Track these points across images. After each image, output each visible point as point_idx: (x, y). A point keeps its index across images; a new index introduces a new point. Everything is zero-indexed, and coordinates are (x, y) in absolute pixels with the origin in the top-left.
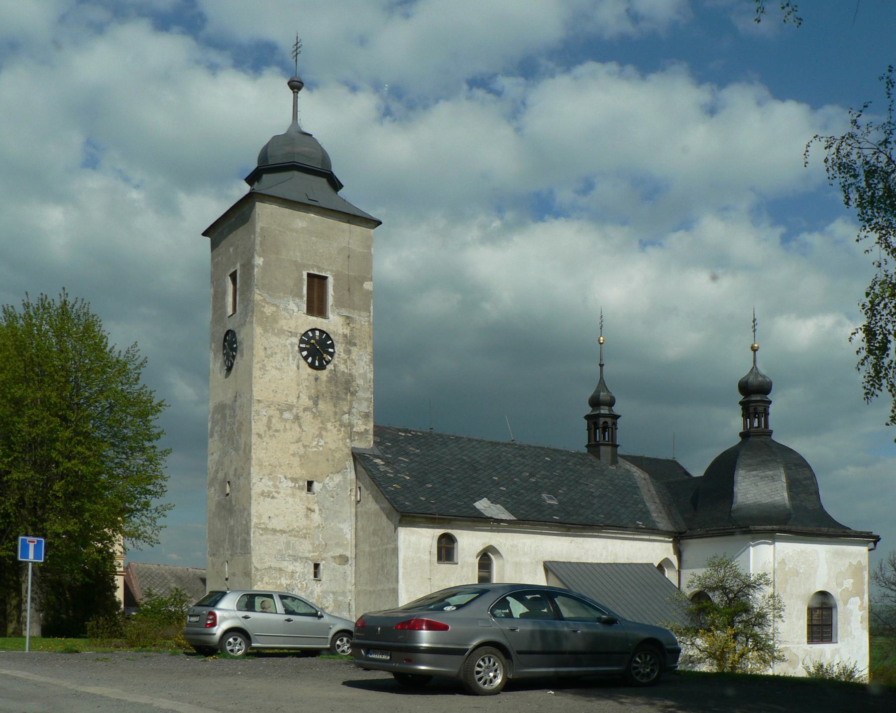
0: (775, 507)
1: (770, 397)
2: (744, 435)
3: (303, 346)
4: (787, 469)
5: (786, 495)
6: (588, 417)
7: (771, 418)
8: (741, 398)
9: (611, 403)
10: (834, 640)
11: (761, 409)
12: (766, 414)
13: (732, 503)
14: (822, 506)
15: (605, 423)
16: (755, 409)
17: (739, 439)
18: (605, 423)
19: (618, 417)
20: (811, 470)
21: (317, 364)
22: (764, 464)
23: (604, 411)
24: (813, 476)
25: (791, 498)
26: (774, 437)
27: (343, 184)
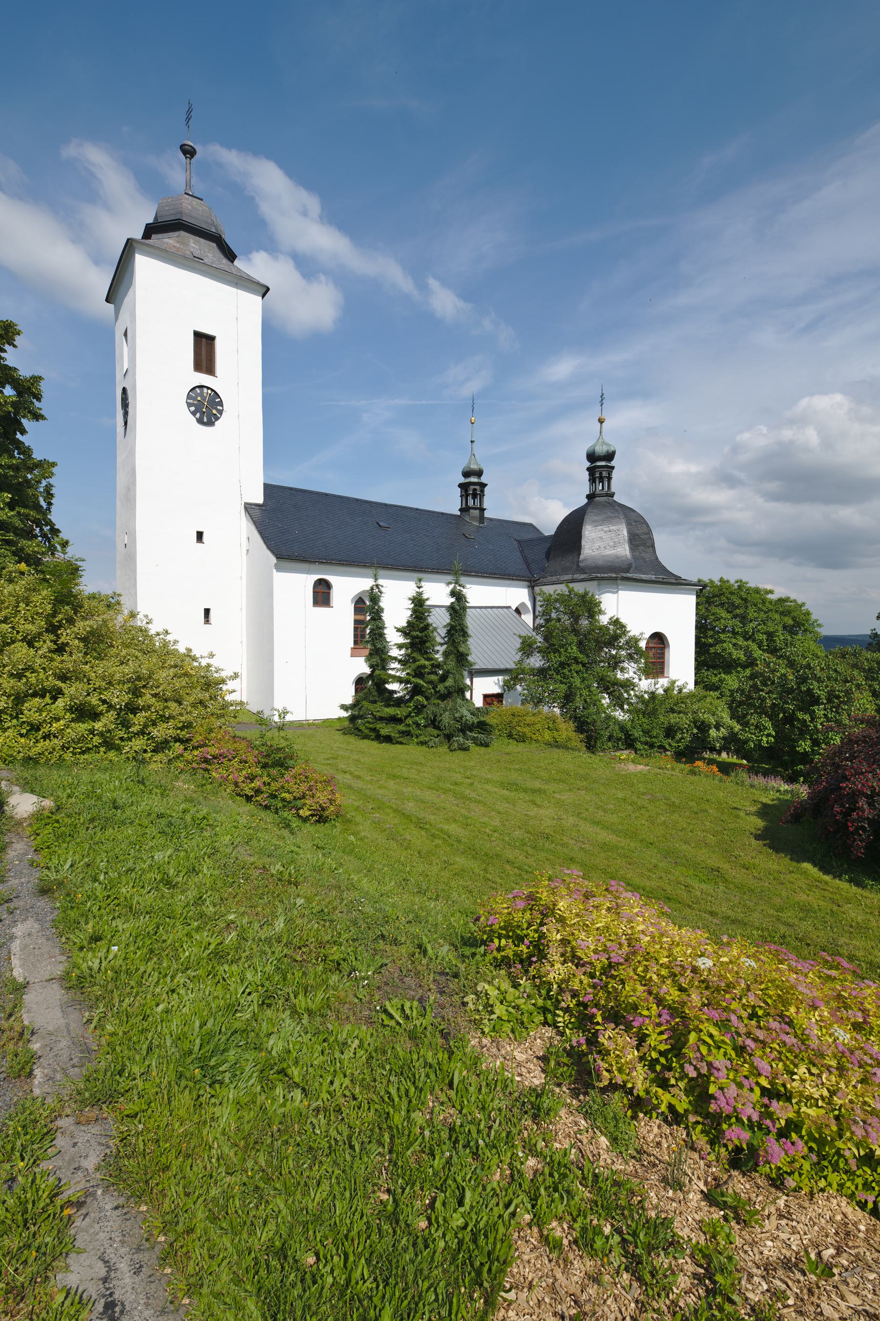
0: (617, 557)
1: (613, 463)
2: (591, 497)
3: (191, 401)
4: (629, 524)
5: (627, 548)
6: (461, 486)
7: (613, 482)
8: (588, 464)
9: (479, 473)
10: (666, 675)
11: (605, 474)
12: (609, 479)
13: (579, 554)
14: (657, 558)
15: (475, 490)
16: (601, 473)
17: (586, 501)
18: (475, 490)
19: (486, 485)
20: (648, 526)
21: (205, 420)
22: (608, 520)
23: (473, 479)
24: (649, 532)
25: (632, 549)
26: (615, 498)
27: (482, 697)
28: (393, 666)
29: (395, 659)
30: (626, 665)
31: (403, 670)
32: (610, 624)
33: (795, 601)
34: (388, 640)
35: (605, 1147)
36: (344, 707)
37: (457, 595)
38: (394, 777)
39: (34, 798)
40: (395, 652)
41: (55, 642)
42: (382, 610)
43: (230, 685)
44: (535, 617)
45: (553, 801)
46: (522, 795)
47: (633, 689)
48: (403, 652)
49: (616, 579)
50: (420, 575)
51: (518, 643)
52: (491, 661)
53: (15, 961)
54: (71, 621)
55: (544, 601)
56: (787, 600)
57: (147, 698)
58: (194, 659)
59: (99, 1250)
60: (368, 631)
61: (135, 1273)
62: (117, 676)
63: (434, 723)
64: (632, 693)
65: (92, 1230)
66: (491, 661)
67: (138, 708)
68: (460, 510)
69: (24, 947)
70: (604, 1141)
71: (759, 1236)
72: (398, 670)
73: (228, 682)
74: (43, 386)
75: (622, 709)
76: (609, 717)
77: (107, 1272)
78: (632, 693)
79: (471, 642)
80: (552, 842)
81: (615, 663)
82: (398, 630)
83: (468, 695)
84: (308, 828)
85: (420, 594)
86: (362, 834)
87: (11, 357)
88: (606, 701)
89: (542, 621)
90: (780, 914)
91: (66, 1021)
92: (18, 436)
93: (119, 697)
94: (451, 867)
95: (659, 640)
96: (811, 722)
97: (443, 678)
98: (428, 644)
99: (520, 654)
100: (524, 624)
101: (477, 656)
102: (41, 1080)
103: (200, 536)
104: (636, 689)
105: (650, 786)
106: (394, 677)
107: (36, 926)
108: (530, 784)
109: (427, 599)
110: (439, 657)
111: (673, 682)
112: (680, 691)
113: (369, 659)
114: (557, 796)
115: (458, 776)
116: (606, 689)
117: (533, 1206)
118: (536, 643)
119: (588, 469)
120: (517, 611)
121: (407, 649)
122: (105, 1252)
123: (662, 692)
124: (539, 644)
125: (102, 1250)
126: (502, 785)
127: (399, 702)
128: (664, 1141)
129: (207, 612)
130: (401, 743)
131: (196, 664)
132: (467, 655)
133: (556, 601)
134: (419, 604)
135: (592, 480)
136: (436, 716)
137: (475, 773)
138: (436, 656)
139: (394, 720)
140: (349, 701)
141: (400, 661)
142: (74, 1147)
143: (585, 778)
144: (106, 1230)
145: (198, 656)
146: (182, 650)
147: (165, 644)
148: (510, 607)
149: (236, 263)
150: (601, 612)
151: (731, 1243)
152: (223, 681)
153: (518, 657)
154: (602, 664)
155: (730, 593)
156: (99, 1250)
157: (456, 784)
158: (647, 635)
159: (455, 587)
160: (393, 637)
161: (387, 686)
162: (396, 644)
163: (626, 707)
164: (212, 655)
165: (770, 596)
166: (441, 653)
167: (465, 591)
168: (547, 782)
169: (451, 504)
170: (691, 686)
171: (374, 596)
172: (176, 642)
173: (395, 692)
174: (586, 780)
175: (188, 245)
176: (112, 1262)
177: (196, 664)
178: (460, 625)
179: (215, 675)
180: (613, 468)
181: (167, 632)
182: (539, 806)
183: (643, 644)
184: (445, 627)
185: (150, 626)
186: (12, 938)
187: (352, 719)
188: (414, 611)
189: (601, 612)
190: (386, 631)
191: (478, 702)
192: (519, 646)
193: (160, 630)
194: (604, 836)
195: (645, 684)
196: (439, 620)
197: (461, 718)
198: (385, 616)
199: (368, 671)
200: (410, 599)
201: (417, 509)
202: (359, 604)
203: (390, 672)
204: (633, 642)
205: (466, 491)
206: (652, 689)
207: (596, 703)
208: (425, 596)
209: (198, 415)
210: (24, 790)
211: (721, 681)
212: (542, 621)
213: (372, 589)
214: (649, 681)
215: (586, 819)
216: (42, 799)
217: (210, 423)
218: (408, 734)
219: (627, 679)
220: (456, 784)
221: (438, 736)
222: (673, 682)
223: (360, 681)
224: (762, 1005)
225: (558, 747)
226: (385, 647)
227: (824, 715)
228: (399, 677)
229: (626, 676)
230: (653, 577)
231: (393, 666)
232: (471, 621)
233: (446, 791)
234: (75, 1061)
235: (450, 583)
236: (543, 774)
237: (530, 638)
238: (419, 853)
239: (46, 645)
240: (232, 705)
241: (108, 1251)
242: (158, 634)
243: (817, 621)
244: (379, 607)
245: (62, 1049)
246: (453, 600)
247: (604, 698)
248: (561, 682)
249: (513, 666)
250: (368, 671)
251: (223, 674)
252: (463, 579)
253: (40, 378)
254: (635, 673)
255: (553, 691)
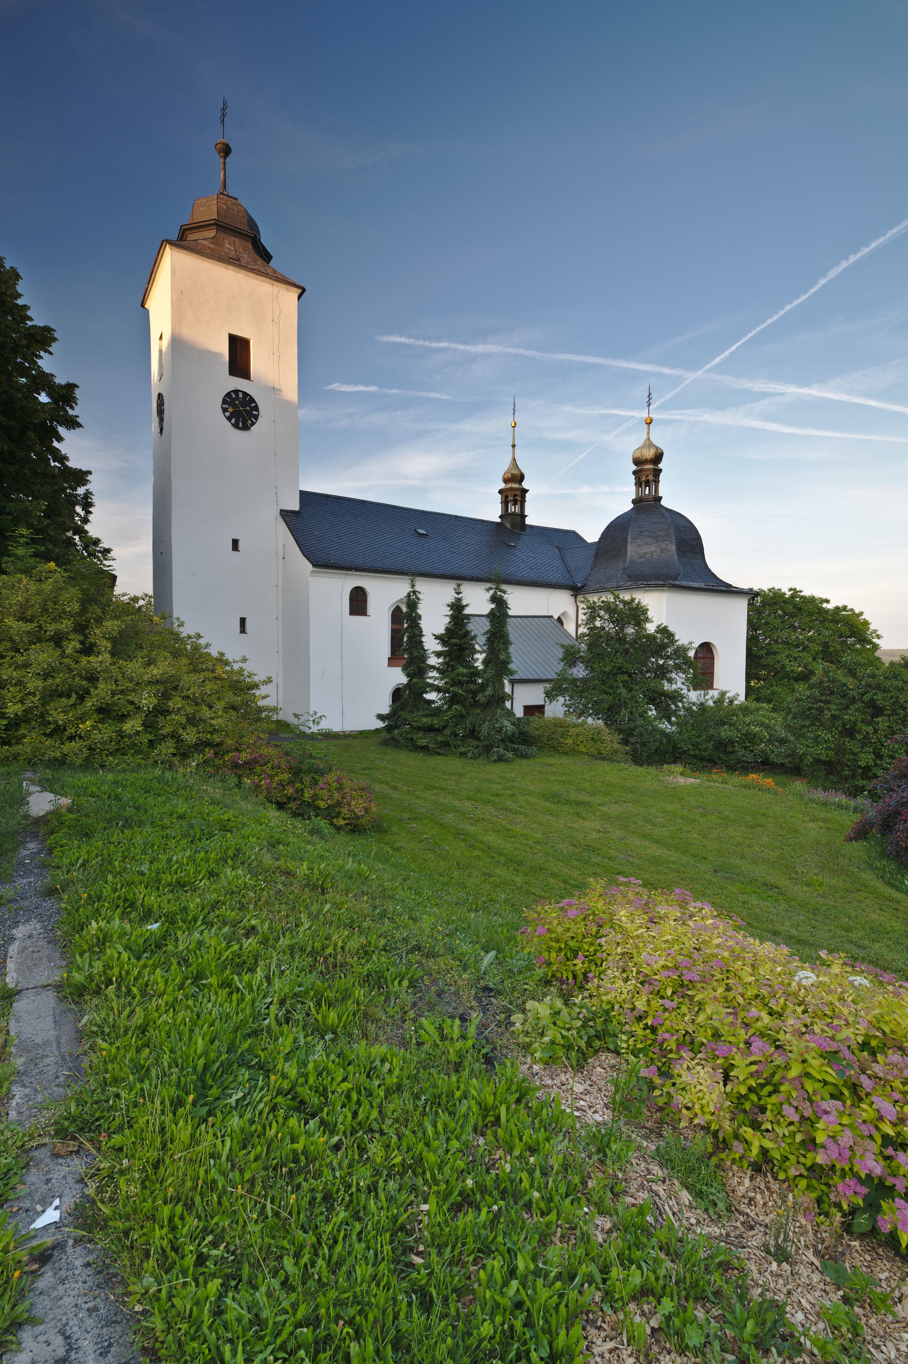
8: (634, 468)
21: (241, 425)
28: (431, 674)
29: (433, 667)
30: (674, 675)
31: (441, 679)
32: (656, 632)
33: (852, 610)
34: (426, 648)
35: (687, 1203)
36: (381, 717)
37: (499, 602)
38: (432, 787)
39: (51, 796)
40: (433, 661)
41: (81, 643)
42: (420, 617)
43: (263, 690)
44: (578, 626)
45: (598, 814)
46: (566, 808)
47: (680, 701)
48: (441, 660)
49: (663, 586)
50: (459, 582)
51: (560, 653)
52: (532, 671)
53: (11, 965)
54: (99, 621)
55: (588, 608)
56: (845, 608)
57: (175, 703)
58: (227, 663)
59: (60, 1320)
60: (405, 639)
61: (101, 1354)
62: (146, 678)
63: (473, 733)
64: (680, 704)
65: (55, 1294)
66: (532, 671)
67: (168, 711)
68: (500, 517)
69: (23, 950)
70: (686, 1197)
71: (892, 1326)
72: (435, 679)
73: (261, 686)
74: (78, 393)
75: (669, 721)
76: (656, 730)
77: (67, 1351)
78: (680, 704)
79: (512, 650)
80: (599, 855)
81: (662, 673)
82: (437, 637)
83: (508, 704)
84: (342, 838)
85: (459, 600)
86: (398, 844)
87: (46, 363)
88: (652, 713)
89: (585, 630)
90: (850, 934)
91: (58, 1032)
92: (55, 444)
93: (147, 700)
94: (491, 880)
95: (706, 649)
96: (873, 733)
97: (483, 687)
98: (467, 652)
99: (562, 664)
100: (567, 634)
101: (519, 662)
102: (19, 1101)
103: (235, 544)
104: (685, 700)
105: (701, 799)
106: (431, 685)
107: (38, 926)
108: (574, 796)
109: (466, 606)
110: (479, 665)
111: (723, 694)
112: (731, 702)
113: (405, 669)
114: (602, 808)
115: (499, 787)
116: (652, 701)
117: (604, 1281)
118: (579, 652)
119: (634, 473)
120: (559, 620)
121: (445, 657)
122: (67, 1323)
123: (712, 704)
124: (582, 654)
125: (64, 1321)
126: (546, 797)
127: (438, 711)
128: (759, 1196)
129: (243, 621)
130: (439, 754)
131: (228, 668)
132: (508, 663)
133: (601, 608)
134: (457, 607)
135: (638, 484)
136: (475, 726)
137: (517, 784)
138: (476, 665)
139: (430, 729)
140: (386, 710)
141: (438, 670)
142: (46, 1184)
143: (631, 790)
144: (73, 1293)
145: (231, 659)
146: (215, 654)
147: (196, 648)
148: (551, 617)
149: (271, 264)
150: (647, 620)
151: (858, 1335)
152: (256, 686)
153: (560, 667)
154: (648, 675)
155: (784, 602)
156: (60, 1320)
157: (497, 795)
158: (696, 645)
159: (495, 593)
160: (431, 644)
161: (425, 695)
162: (434, 652)
163: (673, 719)
164: (244, 660)
165: (825, 605)
166: (480, 661)
167: (505, 596)
168: (592, 794)
169: (492, 512)
170: (742, 698)
171: (412, 602)
172: (208, 645)
173: (433, 702)
174: (632, 792)
175: (223, 246)
176: (75, 1337)
177: (228, 668)
178: (500, 632)
179: (247, 680)
180: (660, 471)
181: (199, 636)
182: (583, 819)
183: (691, 654)
184: (485, 634)
185: (181, 629)
186: (12, 939)
187: (388, 729)
188: (453, 617)
189: (647, 620)
190: (423, 639)
191: (519, 713)
192: (561, 656)
193: (192, 633)
194: (655, 851)
195: (694, 696)
196: (479, 630)
197: (501, 728)
198: (423, 624)
199: (405, 680)
200: (448, 605)
201: (456, 517)
202: (396, 615)
203: (428, 680)
204: (681, 652)
205: (507, 497)
206: (702, 699)
207: (643, 715)
208: (464, 602)
209: (233, 421)
210: (44, 789)
211: (773, 693)
212: (585, 630)
213: (409, 595)
214: (699, 692)
215: (634, 833)
216: (59, 797)
217: (246, 428)
218: (446, 744)
219: (675, 691)
220: (497, 795)
221: (478, 747)
222: (723, 694)
223: (397, 694)
224: (878, 1034)
225: (603, 759)
226: (423, 656)
227: (889, 727)
228: (437, 686)
229: (674, 687)
230: (702, 585)
231: (431, 674)
232: (512, 630)
233: (486, 802)
234: (62, 1079)
235: (491, 589)
236: (587, 786)
237: (572, 647)
238: (458, 864)
239: (72, 645)
240: (265, 711)
241: (71, 1323)
242: (189, 637)
243: (875, 631)
244: (417, 614)
245: (48, 1065)
246: (493, 606)
247: (651, 710)
248: (606, 693)
249: (555, 676)
250: (405, 680)
251: (256, 679)
252: (504, 587)
253: (75, 386)
254: (683, 684)
255: (596, 702)
